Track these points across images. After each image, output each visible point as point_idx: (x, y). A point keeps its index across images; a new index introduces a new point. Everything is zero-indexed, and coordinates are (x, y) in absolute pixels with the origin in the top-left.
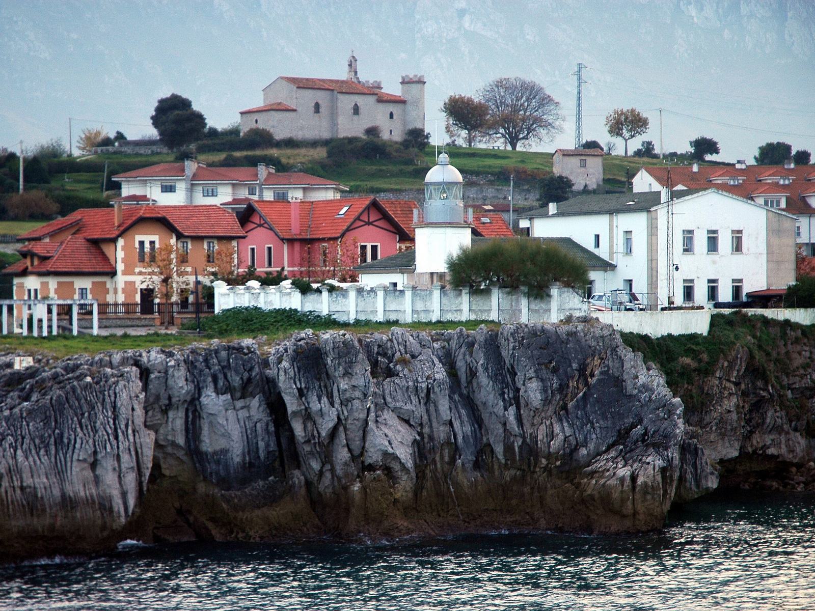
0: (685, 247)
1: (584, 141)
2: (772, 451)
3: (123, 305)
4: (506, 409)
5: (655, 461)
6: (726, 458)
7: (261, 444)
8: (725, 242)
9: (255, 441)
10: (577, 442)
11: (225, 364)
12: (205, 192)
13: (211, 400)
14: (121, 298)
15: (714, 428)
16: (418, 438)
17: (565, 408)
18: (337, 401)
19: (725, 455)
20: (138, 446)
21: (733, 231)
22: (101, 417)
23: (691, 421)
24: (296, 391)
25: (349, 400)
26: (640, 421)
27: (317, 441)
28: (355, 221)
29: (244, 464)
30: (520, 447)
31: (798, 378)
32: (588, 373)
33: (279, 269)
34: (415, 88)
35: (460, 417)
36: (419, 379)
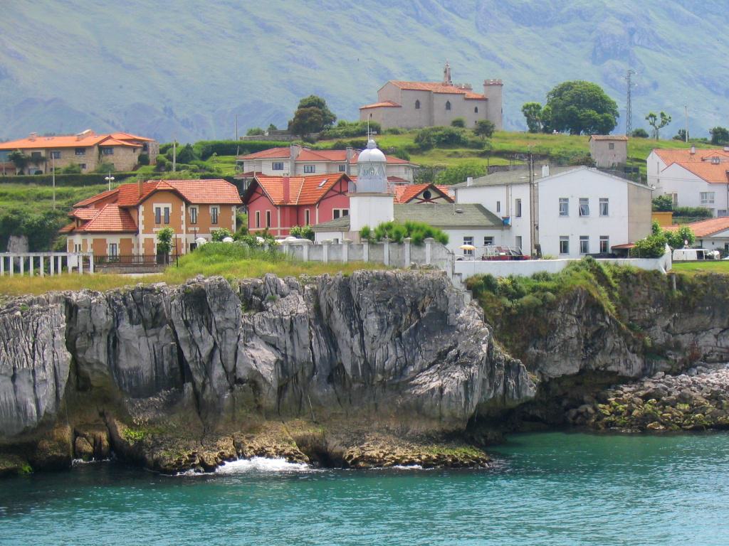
1: (633, 130)
2: (612, 368)
3: (143, 256)
4: (352, 336)
5: (459, 375)
6: (568, 374)
7: (166, 363)
8: (594, 207)
9: (161, 360)
10: (406, 361)
11: (139, 301)
12: (306, 168)
13: (127, 330)
14: (142, 251)
15: (557, 351)
16: (281, 358)
17: (399, 335)
18: (214, 330)
19: (568, 371)
20: (56, 364)
21: (601, 200)
22: (23, 342)
23: (537, 345)
24: (183, 323)
25: (224, 330)
26: (456, 345)
27: (198, 360)
28: (328, 191)
29: (152, 378)
31: (637, 313)
32: (420, 308)
33: (264, 229)
34: (495, 89)
35: (319, 342)
36: (285, 313)
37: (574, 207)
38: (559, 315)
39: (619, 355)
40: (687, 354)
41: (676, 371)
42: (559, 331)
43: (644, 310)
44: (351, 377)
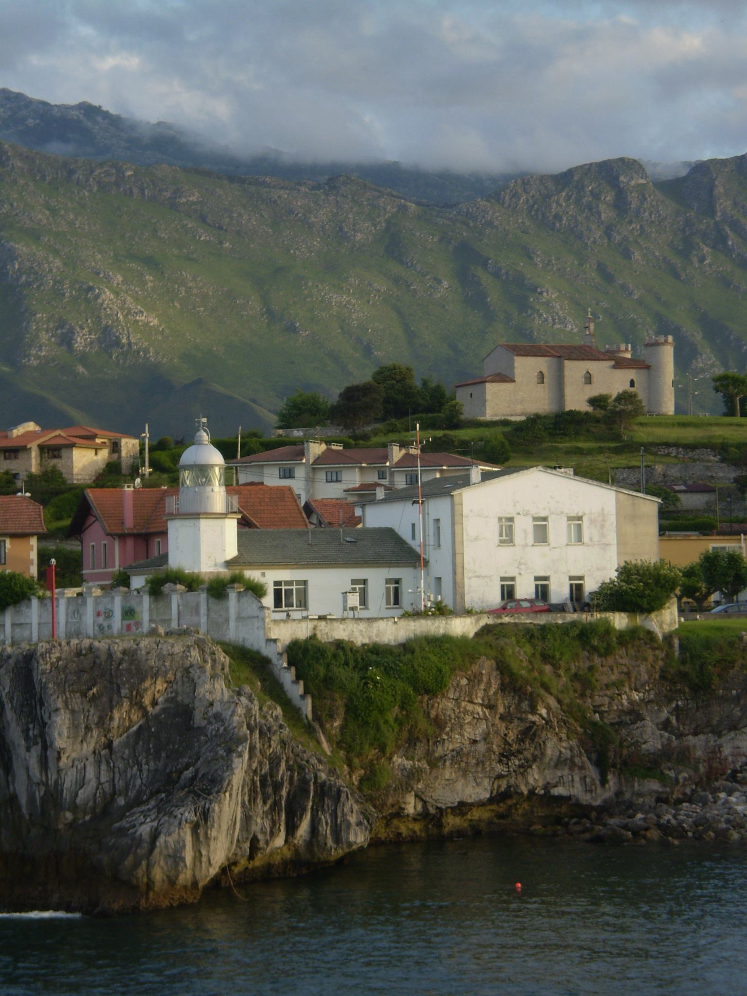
0: (504, 538)
4: (28, 749)
30: (42, 798)
37: (524, 528)
38: (450, 705)
39: (571, 769)
40: (702, 769)
41: (681, 796)
42: (451, 730)
43: (620, 695)
44: (27, 817)
